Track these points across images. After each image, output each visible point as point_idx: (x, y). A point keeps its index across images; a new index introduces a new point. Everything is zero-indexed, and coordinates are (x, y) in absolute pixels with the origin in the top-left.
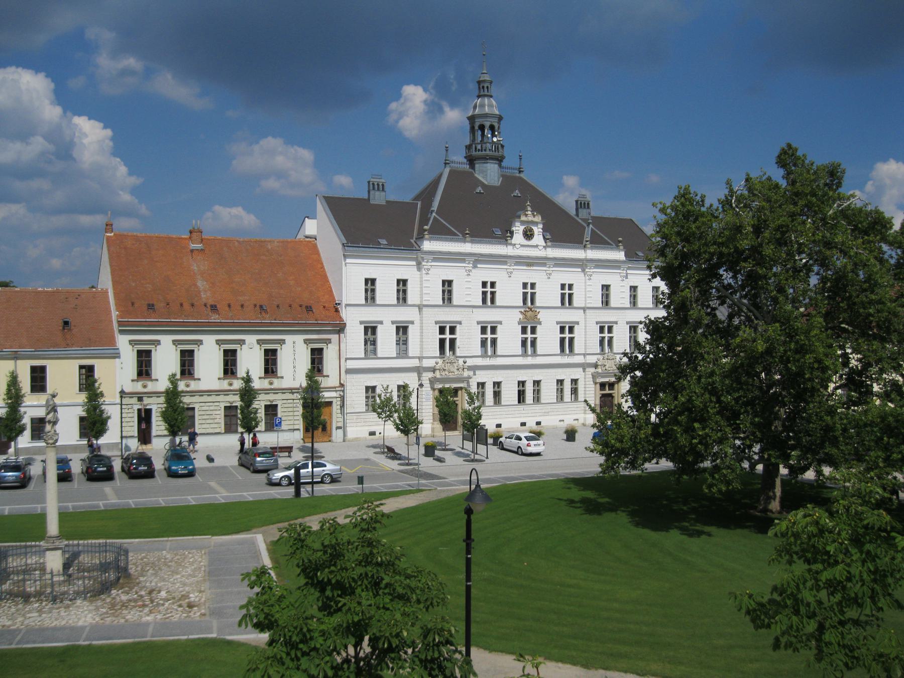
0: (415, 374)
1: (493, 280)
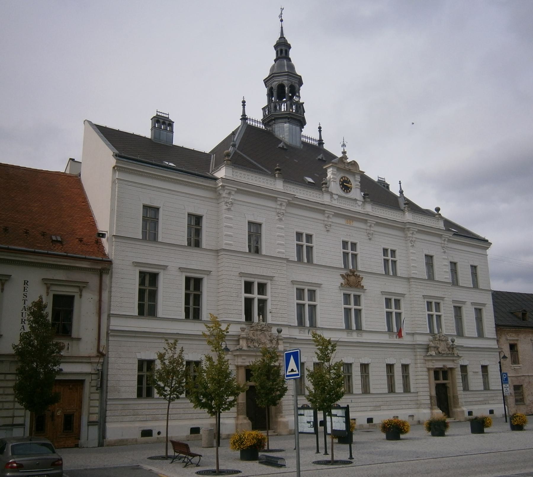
1: (394, 248)
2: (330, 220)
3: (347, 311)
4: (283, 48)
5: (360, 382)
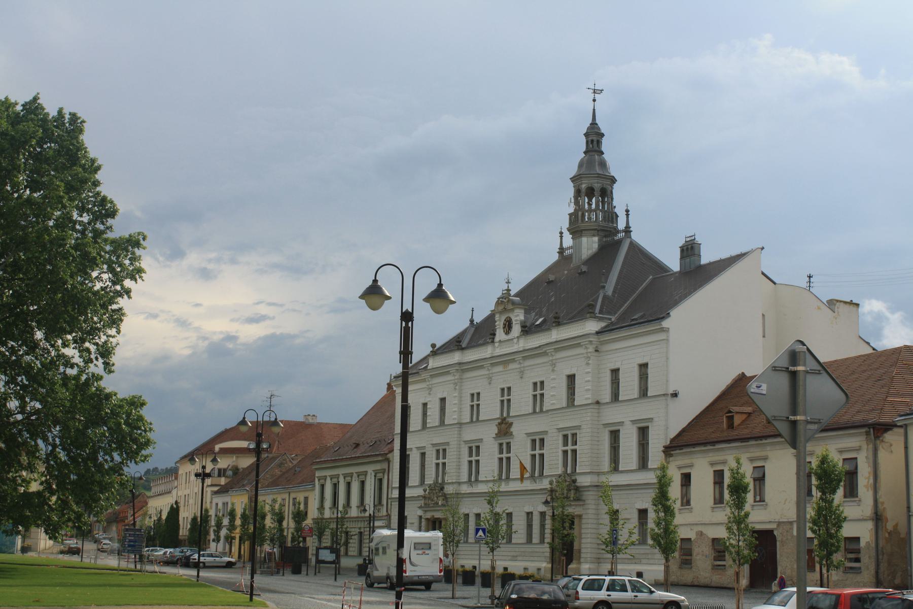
1: (541, 379)
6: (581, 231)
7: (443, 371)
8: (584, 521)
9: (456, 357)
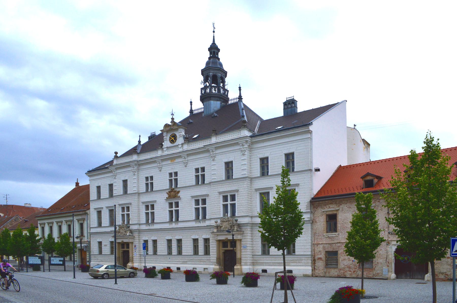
0: (452, 283)
2: (214, 153)
3: (171, 212)
4: (214, 50)
5: (176, 249)
6: (210, 97)
7: (126, 166)
8: (242, 243)
9: (135, 157)
